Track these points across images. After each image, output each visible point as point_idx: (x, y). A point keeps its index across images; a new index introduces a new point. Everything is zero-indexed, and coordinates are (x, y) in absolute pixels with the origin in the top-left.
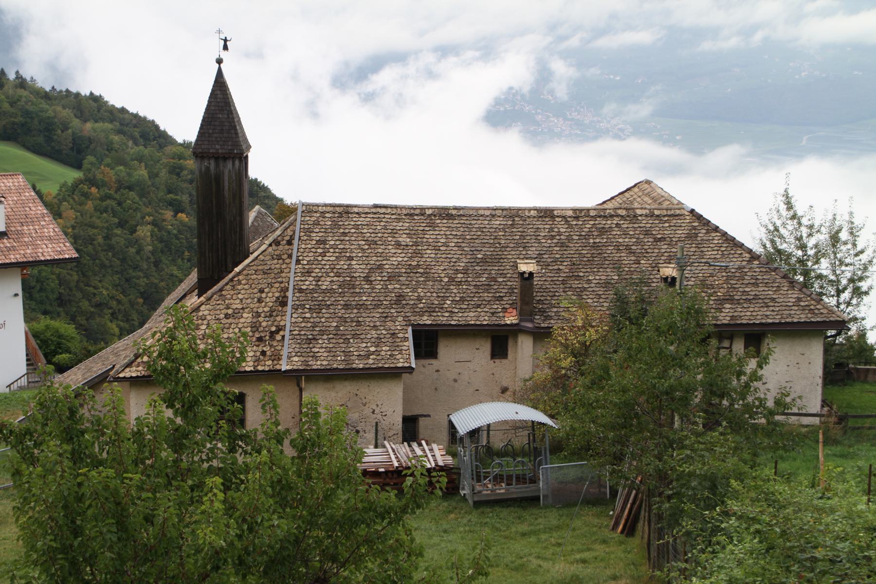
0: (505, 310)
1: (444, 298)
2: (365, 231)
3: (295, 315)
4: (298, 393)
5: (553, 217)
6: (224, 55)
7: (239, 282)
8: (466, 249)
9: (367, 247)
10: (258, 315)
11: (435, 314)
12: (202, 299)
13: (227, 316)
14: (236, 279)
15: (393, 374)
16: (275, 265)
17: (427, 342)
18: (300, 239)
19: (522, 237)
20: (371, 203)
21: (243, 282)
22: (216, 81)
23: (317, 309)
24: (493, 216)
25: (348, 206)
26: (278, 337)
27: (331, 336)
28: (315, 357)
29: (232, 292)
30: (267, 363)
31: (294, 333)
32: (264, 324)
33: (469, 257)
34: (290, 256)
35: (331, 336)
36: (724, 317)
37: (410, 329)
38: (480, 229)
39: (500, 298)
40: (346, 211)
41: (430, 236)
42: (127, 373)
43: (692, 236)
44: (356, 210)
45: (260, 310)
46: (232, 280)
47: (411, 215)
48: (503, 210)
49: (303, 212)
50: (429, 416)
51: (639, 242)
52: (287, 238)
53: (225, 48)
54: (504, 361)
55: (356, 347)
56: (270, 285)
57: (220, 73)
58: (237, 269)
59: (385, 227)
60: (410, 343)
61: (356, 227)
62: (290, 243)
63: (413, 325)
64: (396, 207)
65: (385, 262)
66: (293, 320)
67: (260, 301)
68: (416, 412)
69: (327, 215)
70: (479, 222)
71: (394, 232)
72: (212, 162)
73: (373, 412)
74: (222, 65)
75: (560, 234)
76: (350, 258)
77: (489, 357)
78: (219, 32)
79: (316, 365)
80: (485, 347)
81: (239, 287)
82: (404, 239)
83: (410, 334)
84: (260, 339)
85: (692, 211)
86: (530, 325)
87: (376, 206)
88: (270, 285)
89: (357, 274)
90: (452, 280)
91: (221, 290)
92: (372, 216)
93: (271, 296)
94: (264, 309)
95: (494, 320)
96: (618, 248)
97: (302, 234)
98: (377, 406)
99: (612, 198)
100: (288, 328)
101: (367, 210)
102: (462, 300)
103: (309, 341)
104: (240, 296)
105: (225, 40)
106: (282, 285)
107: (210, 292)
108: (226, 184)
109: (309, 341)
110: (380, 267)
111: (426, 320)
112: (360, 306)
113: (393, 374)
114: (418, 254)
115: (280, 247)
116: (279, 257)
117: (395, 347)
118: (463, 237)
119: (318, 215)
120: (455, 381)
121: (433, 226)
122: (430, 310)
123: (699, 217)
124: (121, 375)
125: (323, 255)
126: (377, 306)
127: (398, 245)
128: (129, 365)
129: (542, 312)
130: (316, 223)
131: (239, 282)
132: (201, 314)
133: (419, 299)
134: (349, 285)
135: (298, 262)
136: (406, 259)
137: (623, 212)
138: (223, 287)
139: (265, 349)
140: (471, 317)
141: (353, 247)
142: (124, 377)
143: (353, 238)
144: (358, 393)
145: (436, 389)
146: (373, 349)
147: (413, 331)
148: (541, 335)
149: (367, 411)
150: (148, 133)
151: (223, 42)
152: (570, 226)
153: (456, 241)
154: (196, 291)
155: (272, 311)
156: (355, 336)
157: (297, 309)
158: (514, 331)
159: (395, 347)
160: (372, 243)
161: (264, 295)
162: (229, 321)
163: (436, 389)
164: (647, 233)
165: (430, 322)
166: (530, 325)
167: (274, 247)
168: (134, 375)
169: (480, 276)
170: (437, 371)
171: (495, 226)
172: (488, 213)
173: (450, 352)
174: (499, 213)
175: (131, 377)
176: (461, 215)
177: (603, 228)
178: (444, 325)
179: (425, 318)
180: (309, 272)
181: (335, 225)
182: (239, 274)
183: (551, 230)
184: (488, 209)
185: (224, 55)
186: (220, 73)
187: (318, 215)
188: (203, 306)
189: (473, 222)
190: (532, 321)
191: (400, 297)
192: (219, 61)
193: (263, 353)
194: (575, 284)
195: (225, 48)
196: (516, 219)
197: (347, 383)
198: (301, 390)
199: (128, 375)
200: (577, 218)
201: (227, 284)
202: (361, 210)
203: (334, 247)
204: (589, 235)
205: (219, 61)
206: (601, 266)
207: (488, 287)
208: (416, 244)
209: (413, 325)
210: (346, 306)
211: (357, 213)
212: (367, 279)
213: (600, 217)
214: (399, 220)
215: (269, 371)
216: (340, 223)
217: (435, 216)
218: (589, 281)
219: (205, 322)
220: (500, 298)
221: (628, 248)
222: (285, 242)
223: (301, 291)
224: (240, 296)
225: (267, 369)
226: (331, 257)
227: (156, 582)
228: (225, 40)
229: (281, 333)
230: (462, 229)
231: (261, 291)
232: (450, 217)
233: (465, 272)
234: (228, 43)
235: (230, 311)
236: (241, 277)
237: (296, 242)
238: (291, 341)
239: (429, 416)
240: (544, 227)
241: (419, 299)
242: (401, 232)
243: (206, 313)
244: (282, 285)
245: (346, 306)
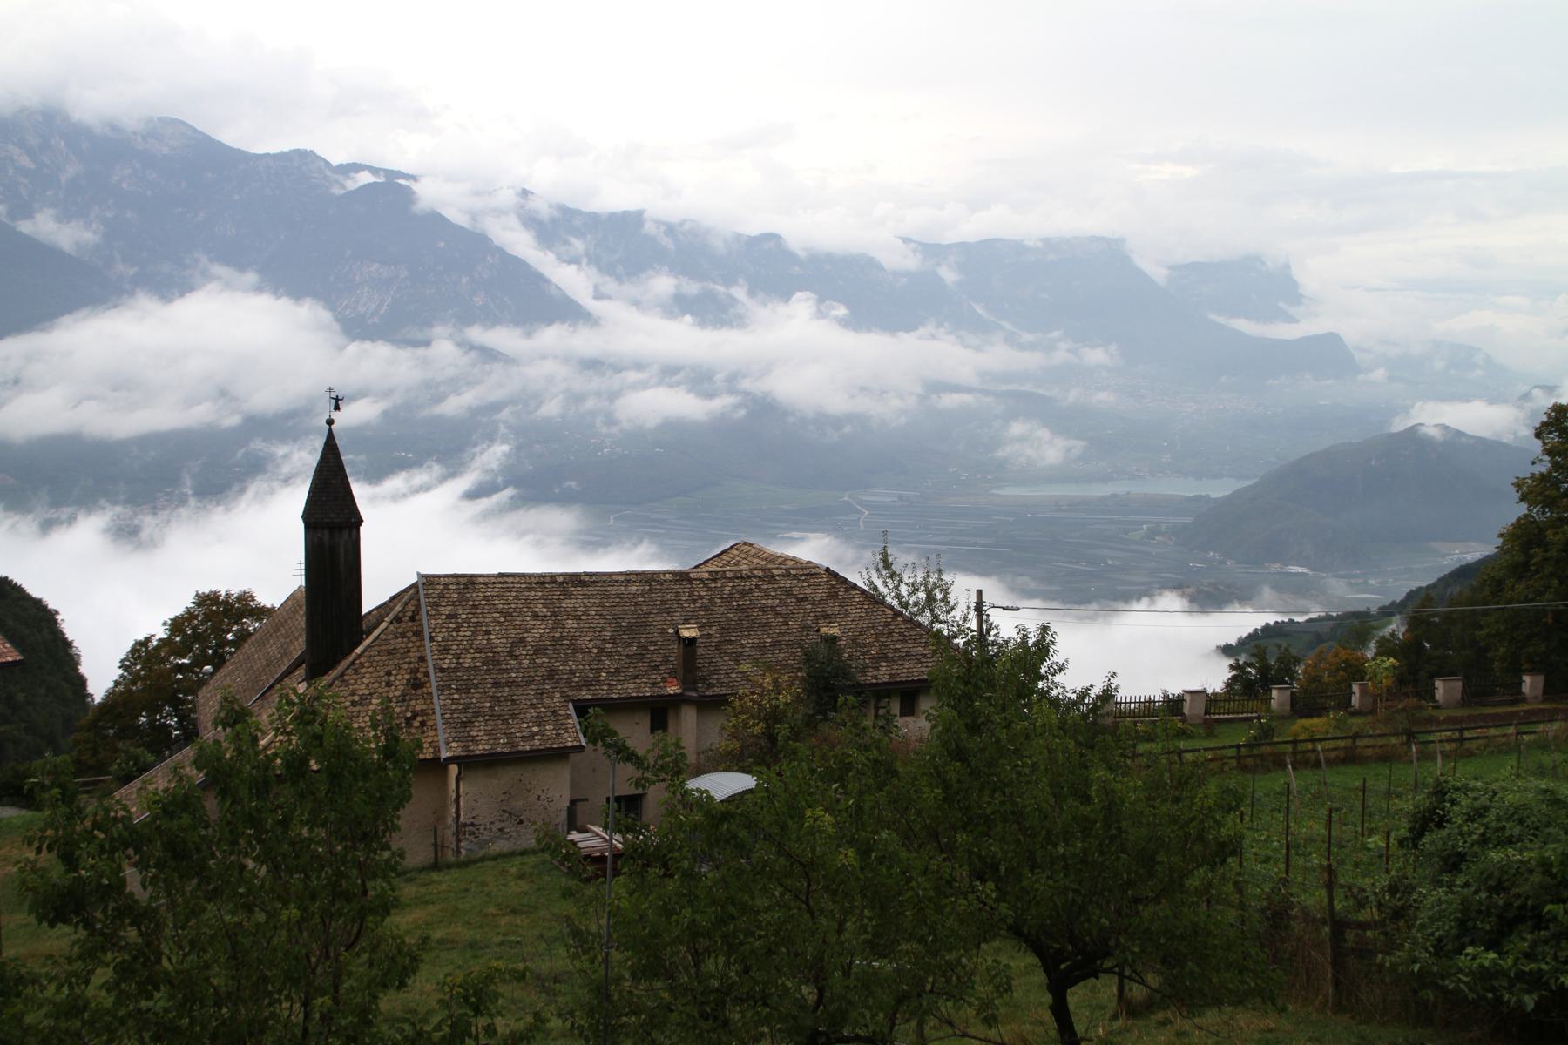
0: (664, 680)
1: (599, 671)
5: (690, 580)
6: (335, 415)
7: (362, 666)
10: (390, 700)
13: (354, 704)
15: (559, 755)
16: (400, 643)
19: (664, 602)
20: (496, 572)
22: (327, 444)
23: (465, 688)
25: (472, 576)
28: (477, 743)
32: (397, 710)
36: (883, 674)
38: (618, 596)
39: (656, 668)
40: (470, 581)
41: (567, 604)
43: (832, 595)
46: (353, 663)
47: (543, 583)
51: (782, 603)
55: (519, 729)
56: (398, 667)
58: (358, 651)
59: (517, 598)
61: (486, 598)
64: (524, 575)
67: (388, 684)
71: (528, 603)
72: (326, 532)
75: (701, 597)
76: (488, 633)
78: (330, 390)
79: (479, 749)
80: (645, 721)
82: (540, 609)
83: (572, 711)
85: (828, 569)
87: (502, 575)
88: (398, 667)
90: (601, 651)
91: (342, 675)
93: (401, 679)
95: (656, 691)
96: (762, 608)
99: (706, 562)
102: (618, 671)
103: (464, 725)
108: (342, 555)
109: (464, 725)
110: (522, 640)
112: (511, 684)
113: (559, 755)
114: (558, 624)
116: (403, 635)
117: (559, 725)
118: (601, 604)
121: (568, 594)
122: (587, 684)
123: (835, 575)
125: (457, 630)
126: (529, 683)
127: (535, 616)
129: (703, 680)
130: (442, 596)
131: (362, 666)
133: (572, 672)
134: (493, 661)
135: (432, 639)
137: (760, 573)
140: (631, 689)
146: (535, 729)
148: (711, 704)
152: (710, 589)
155: (404, 695)
156: (513, 716)
158: (676, 702)
159: (559, 725)
160: (507, 615)
164: (789, 593)
169: (629, 645)
172: (622, 578)
174: (633, 578)
180: (446, 650)
181: (462, 598)
182: (360, 656)
183: (691, 594)
184: (621, 573)
185: (335, 415)
186: (330, 435)
190: (696, 690)
191: (552, 672)
194: (730, 649)
200: (714, 580)
203: (468, 621)
204: (730, 598)
206: (750, 629)
207: (641, 657)
208: (554, 614)
210: (496, 684)
212: (511, 653)
214: (530, 589)
218: (742, 646)
220: (656, 668)
221: (773, 609)
223: (442, 670)
226: (466, 632)
227: (1564, 902)
228: (337, 399)
231: (389, 674)
233: (613, 641)
235: (356, 698)
240: (684, 589)
241: (572, 672)
245: (496, 684)
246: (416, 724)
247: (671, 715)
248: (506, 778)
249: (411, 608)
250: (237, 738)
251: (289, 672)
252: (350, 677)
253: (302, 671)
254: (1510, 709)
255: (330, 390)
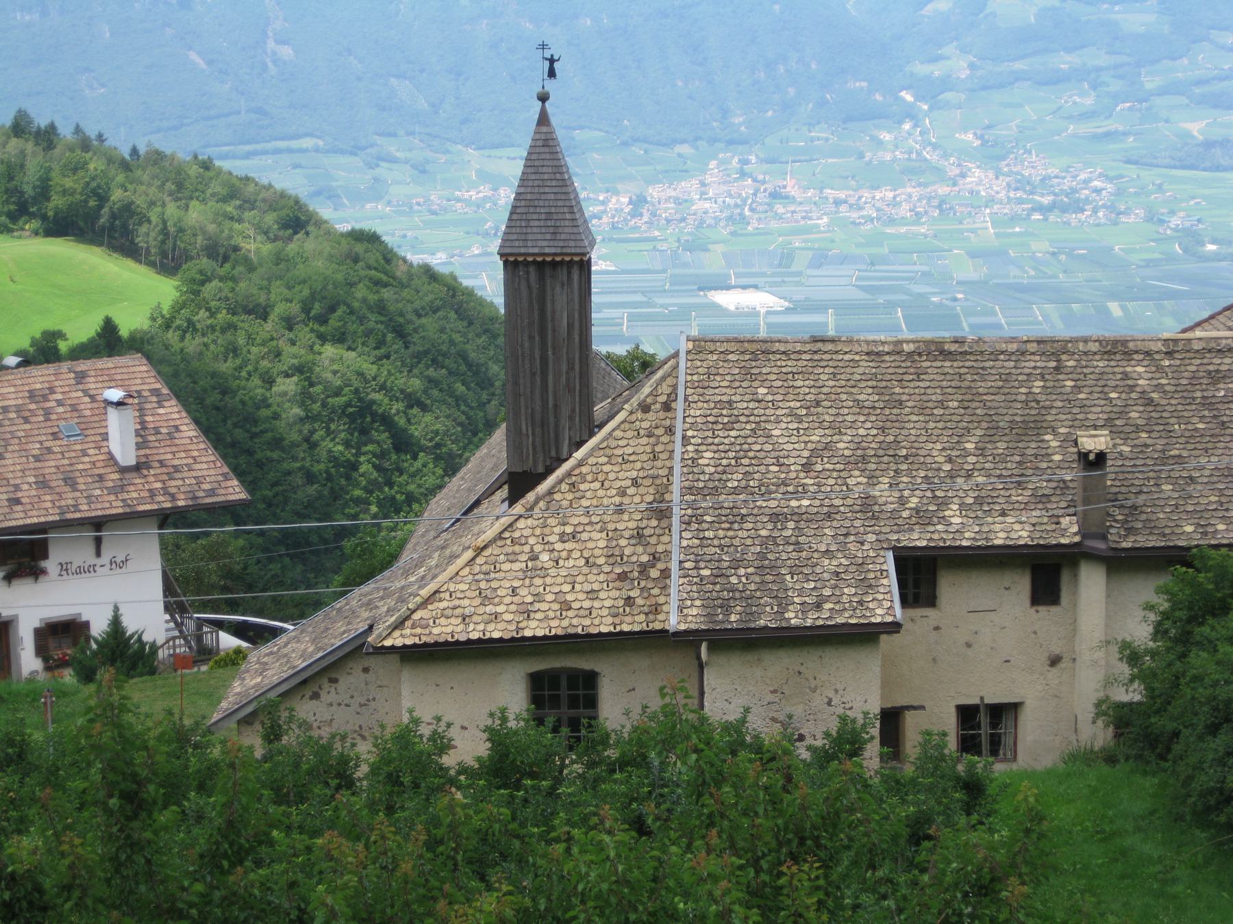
2: (800, 383)
3: (686, 535)
4: (696, 674)
6: (550, 86)
8: (979, 411)
9: (804, 412)
11: (931, 528)
12: (518, 508)
14: (576, 472)
17: (920, 574)
18: (686, 400)
21: (589, 478)
24: (1023, 354)
26: (654, 573)
27: (750, 570)
29: (570, 496)
30: (637, 618)
31: (687, 565)
33: (984, 425)
34: (670, 431)
35: (750, 570)
37: (890, 555)
42: (397, 640)
44: (782, 348)
45: (621, 526)
46: (569, 474)
48: (1039, 342)
49: (688, 352)
50: (922, 708)
52: (663, 399)
53: (552, 73)
54: (1054, 609)
57: (543, 119)
58: (579, 455)
60: (892, 581)
62: (667, 407)
63: (894, 549)
65: (836, 438)
66: (685, 543)
68: (900, 701)
69: (731, 357)
70: (999, 364)
73: (829, 703)
74: (547, 104)
77: (1028, 602)
78: (543, 46)
80: (1022, 584)
81: (582, 487)
83: (890, 566)
84: (623, 577)
86: (1101, 545)
89: (792, 460)
91: (550, 492)
92: (808, 357)
94: (627, 524)
97: (690, 391)
98: (836, 691)
100: (676, 557)
101: (799, 347)
104: (585, 503)
105: (552, 61)
106: (658, 482)
107: (531, 496)
111: (918, 539)
113: (864, 636)
115: (650, 416)
119: (715, 357)
120: (969, 645)
124: (388, 643)
128: (399, 625)
132: (517, 534)
136: (874, 432)
138: (553, 487)
139: (632, 594)
141: (779, 412)
142: (393, 647)
143: (780, 397)
144: (802, 669)
145: (934, 660)
147: (896, 559)
149: (818, 701)
150: (452, 296)
151: (547, 64)
153: (960, 398)
154: (506, 487)
157: (689, 523)
161: (626, 500)
162: (569, 546)
163: (934, 660)
165: (924, 543)
166: (1101, 545)
167: (639, 415)
168: (409, 642)
170: (937, 628)
171: (1027, 371)
173: (955, 593)
174: (1032, 347)
175: (405, 646)
176: (965, 353)
177: (1217, 371)
178: (950, 547)
179: (915, 536)
182: (580, 464)
185: (550, 86)
186: (543, 119)
187: (715, 357)
188: (522, 520)
189: (988, 364)
192: (543, 98)
193: (629, 601)
195: (552, 73)
196: (1064, 357)
197: (782, 653)
198: (701, 667)
199: (399, 642)
200: (1170, 354)
201: (560, 481)
202: (789, 347)
205: (543, 98)
209: (894, 549)
211: (784, 353)
213: (1210, 351)
215: (641, 632)
216: (755, 371)
217: (920, 354)
219: (527, 548)
222: (658, 406)
224: (585, 503)
225: (637, 628)
228: (552, 61)
229: (660, 566)
230: (969, 377)
232: (946, 355)
234: (556, 65)
236: (584, 470)
237: (679, 405)
238: (682, 581)
239: (922, 708)
242: (863, 384)
243: (527, 532)
244: (658, 482)
246: (654, 573)
247: (1065, 577)
248: (778, 664)
249: (665, 388)
250: (662, 763)
251: (489, 493)
252: (564, 497)
253: (504, 492)
254: (549, 344)
255: (543, 46)
